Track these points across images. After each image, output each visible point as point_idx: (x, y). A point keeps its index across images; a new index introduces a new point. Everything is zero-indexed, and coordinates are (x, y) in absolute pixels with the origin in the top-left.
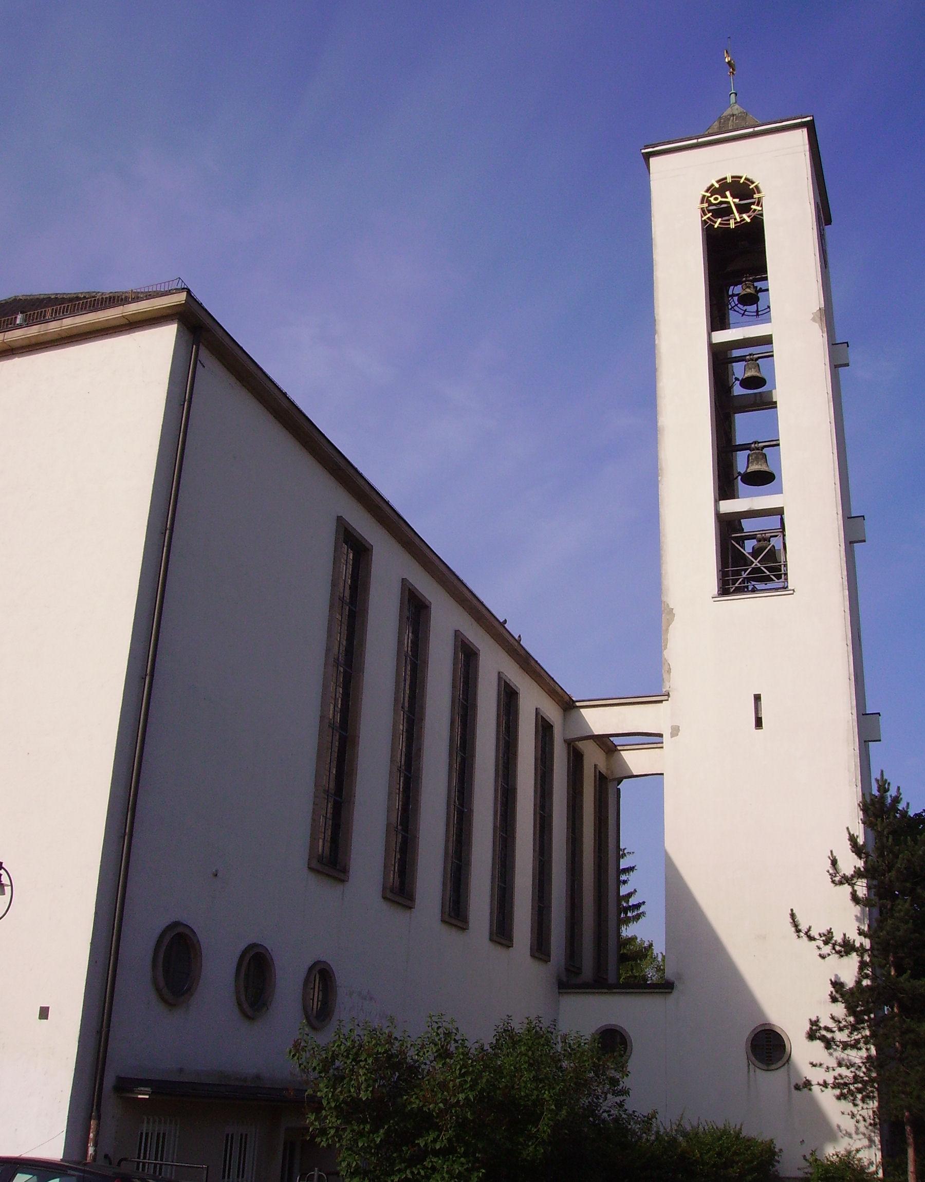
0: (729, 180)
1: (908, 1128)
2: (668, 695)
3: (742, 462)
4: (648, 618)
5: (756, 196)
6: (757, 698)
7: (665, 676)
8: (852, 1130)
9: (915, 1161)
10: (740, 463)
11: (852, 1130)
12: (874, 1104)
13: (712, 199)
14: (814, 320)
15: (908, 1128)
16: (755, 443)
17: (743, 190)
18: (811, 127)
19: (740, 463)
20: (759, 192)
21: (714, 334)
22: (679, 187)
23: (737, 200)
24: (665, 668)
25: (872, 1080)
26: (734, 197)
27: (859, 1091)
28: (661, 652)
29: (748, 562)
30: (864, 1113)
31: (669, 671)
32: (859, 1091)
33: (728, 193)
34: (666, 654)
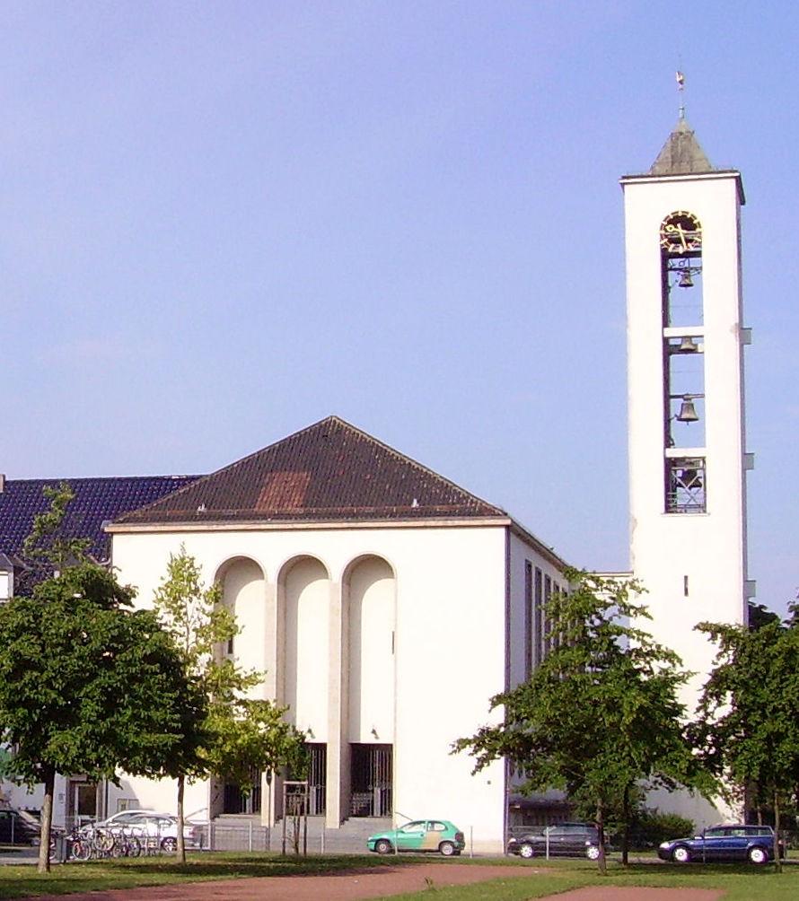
0: (695, 222)
1: (759, 815)
2: (633, 572)
3: (676, 405)
4: (622, 523)
5: (698, 230)
6: (686, 578)
7: (631, 561)
8: (730, 816)
9: (688, 446)
10: (680, 409)
11: (730, 816)
12: (742, 803)
13: (668, 228)
14: (731, 331)
15: (759, 815)
16: (687, 395)
17: (687, 222)
18: (738, 179)
19: (680, 409)
20: (700, 227)
21: (666, 329)
22: (646, 209)
23: (685, 232)
24: (631, 557)
25: (742, 791)
26: (683, 228)
27: (736, 796)
28: (629, 513)
29: (682, 479)
30: (738, 807)
31: (634, 558)
32: (736, 796)
33: (679, 225)
34: (632, 547)
